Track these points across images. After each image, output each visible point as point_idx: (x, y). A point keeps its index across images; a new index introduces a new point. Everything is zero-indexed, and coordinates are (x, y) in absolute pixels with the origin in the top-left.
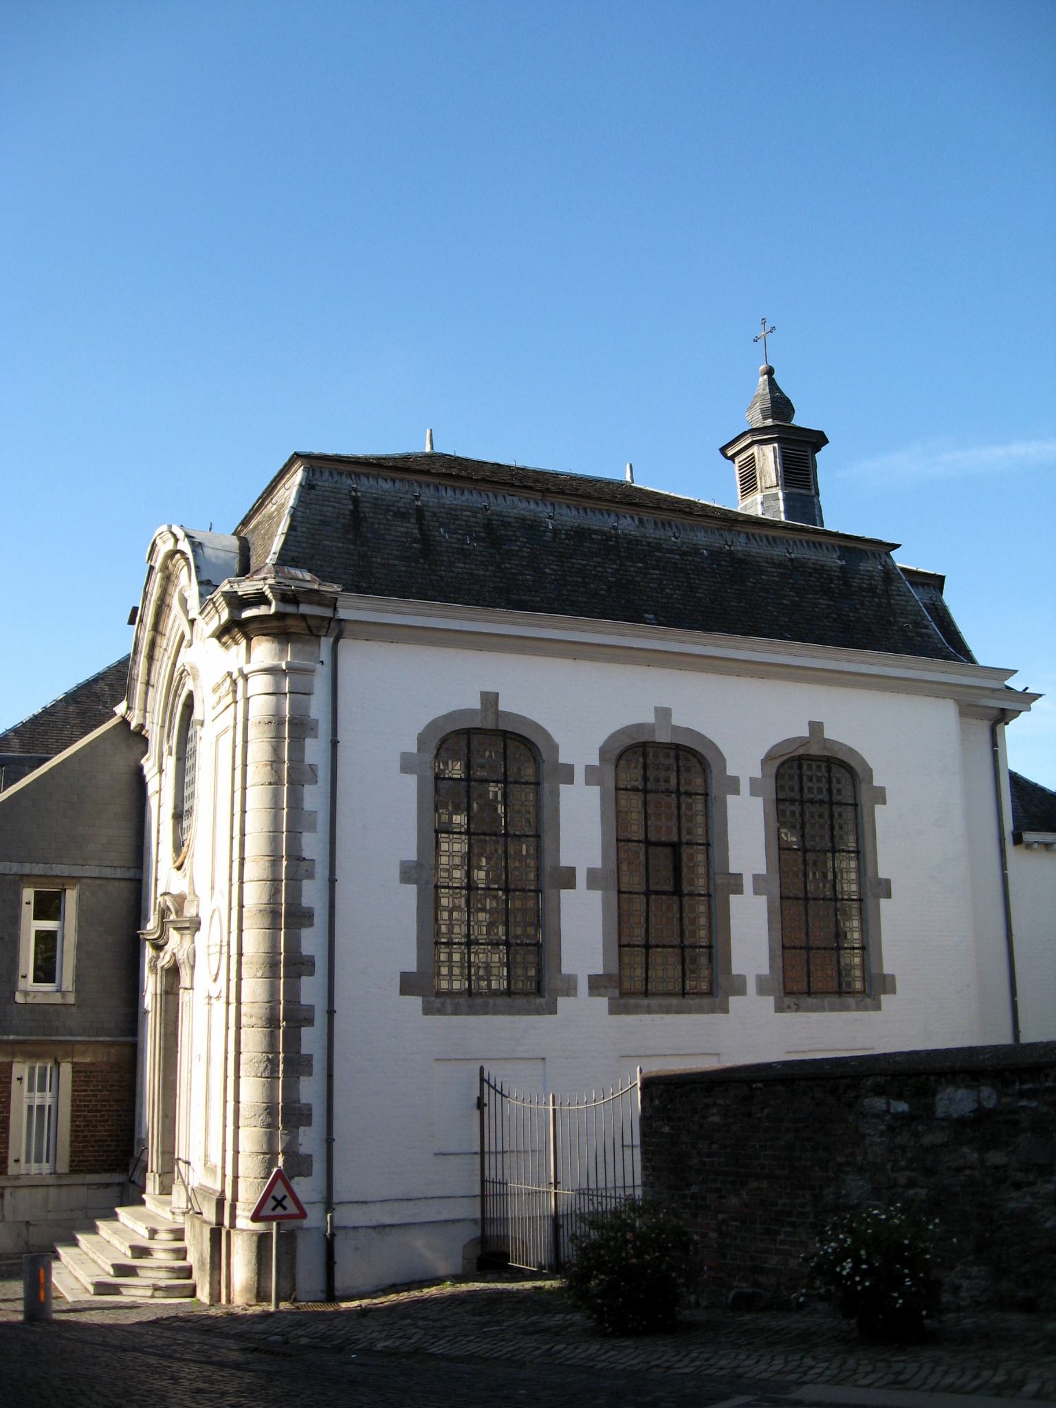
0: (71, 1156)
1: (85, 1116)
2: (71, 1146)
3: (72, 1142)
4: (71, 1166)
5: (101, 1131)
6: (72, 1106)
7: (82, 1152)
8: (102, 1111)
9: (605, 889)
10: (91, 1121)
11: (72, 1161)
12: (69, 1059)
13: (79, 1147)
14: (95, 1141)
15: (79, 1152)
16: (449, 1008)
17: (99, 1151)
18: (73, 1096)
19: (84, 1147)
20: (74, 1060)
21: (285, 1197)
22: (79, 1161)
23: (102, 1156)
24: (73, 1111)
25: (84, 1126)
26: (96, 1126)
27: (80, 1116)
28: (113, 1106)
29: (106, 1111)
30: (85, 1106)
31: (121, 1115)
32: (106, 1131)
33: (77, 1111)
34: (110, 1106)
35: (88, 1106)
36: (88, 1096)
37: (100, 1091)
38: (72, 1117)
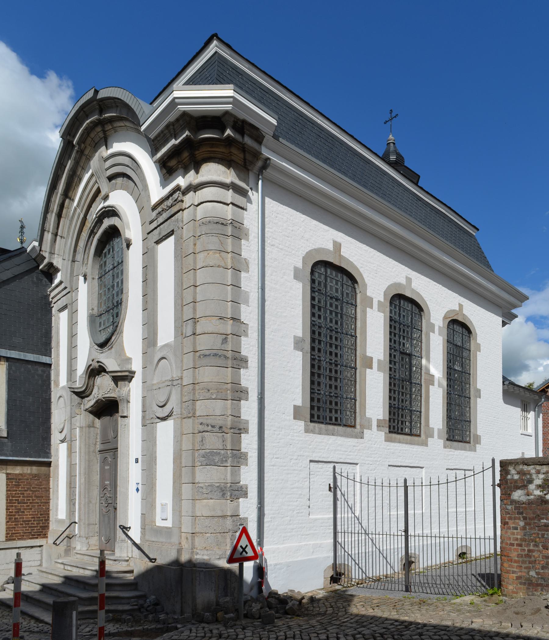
0: (7, 531)
1: (15, 506)
2: (7, 525)
3: (7, 522)
4: (7, 537)
5: (27, 515)
6: (7, 500)
7: (15, 528)
8: (27, 503)
9: (384, 372)
10: (20, 509)
11: (7, 534)
12: (4, 471)
13: (12, 525)
14: (23, 521)
15: (13, 528)
16: (317, 430)
17: (26, 527)
18: (7, 494)
19: (15, 525)
20: (8, 472)
21: (247, 546)
22: (12, 534)
23: (28, 530)
24: (7, 503)
25: (15, 512)
26: (24, 512)
27: (12, 506)
28: (35, 500)
29: (30, 503)
30: (16, 500)
31: (40, 506)
32: (30, 515)
33: (10, 503)
34: (33, 500)
35: (18, 500)
36: (18, 494)
37: (26, 491)
38: (7, 506)
